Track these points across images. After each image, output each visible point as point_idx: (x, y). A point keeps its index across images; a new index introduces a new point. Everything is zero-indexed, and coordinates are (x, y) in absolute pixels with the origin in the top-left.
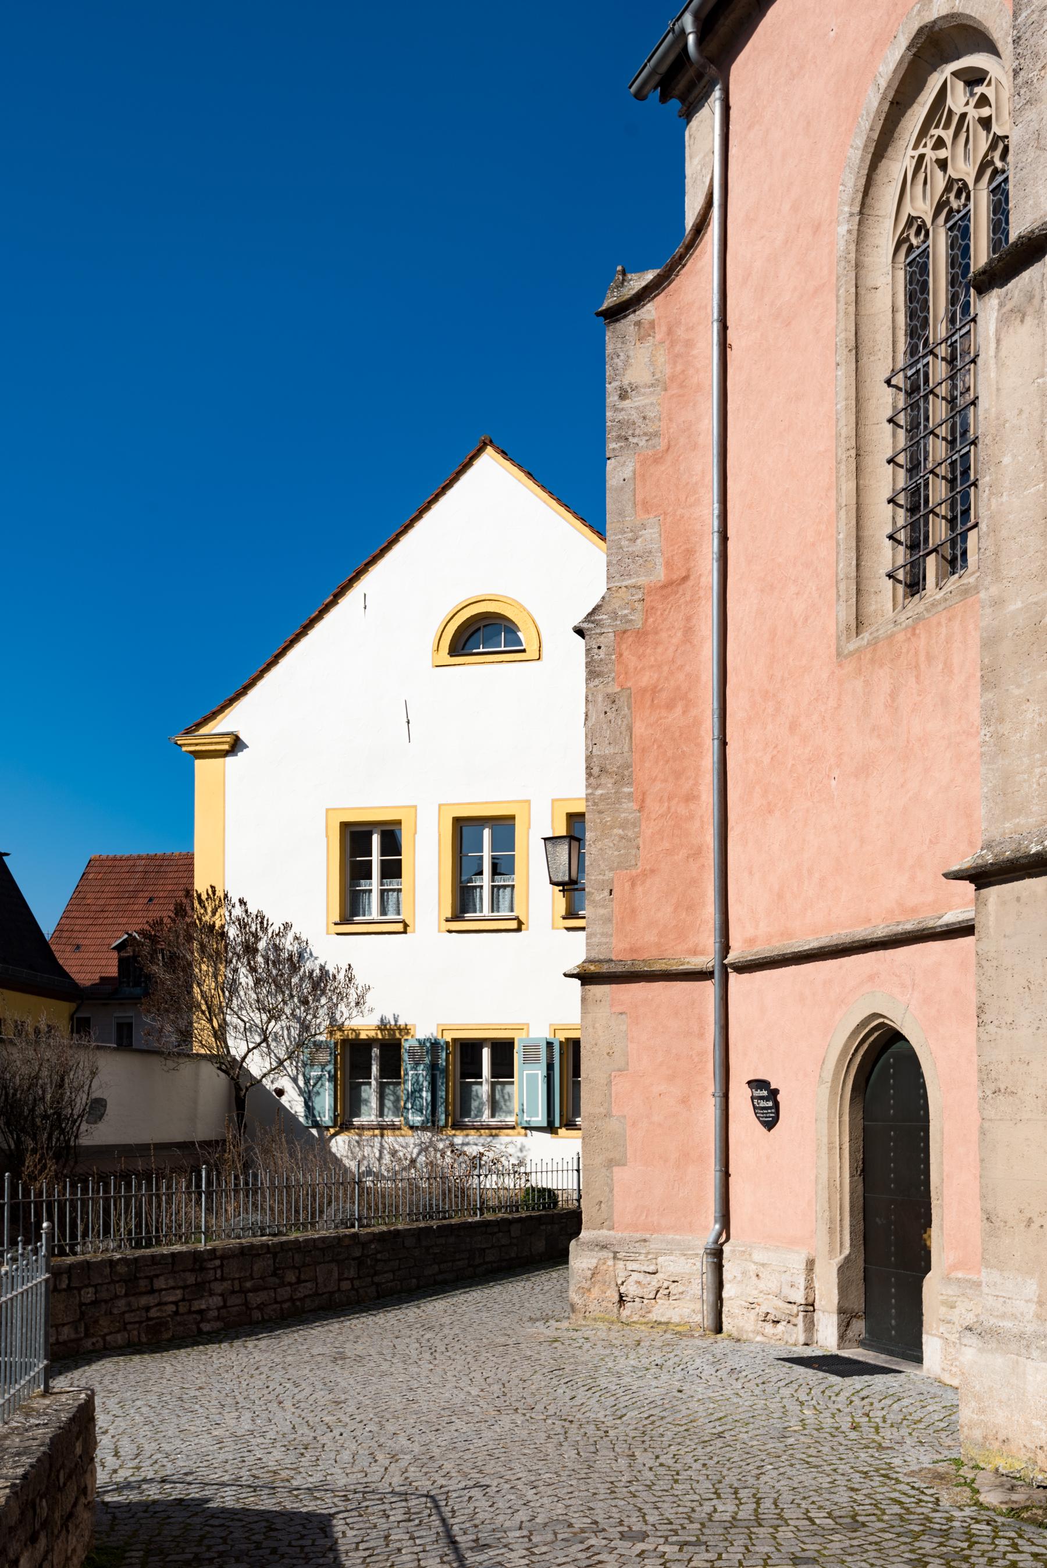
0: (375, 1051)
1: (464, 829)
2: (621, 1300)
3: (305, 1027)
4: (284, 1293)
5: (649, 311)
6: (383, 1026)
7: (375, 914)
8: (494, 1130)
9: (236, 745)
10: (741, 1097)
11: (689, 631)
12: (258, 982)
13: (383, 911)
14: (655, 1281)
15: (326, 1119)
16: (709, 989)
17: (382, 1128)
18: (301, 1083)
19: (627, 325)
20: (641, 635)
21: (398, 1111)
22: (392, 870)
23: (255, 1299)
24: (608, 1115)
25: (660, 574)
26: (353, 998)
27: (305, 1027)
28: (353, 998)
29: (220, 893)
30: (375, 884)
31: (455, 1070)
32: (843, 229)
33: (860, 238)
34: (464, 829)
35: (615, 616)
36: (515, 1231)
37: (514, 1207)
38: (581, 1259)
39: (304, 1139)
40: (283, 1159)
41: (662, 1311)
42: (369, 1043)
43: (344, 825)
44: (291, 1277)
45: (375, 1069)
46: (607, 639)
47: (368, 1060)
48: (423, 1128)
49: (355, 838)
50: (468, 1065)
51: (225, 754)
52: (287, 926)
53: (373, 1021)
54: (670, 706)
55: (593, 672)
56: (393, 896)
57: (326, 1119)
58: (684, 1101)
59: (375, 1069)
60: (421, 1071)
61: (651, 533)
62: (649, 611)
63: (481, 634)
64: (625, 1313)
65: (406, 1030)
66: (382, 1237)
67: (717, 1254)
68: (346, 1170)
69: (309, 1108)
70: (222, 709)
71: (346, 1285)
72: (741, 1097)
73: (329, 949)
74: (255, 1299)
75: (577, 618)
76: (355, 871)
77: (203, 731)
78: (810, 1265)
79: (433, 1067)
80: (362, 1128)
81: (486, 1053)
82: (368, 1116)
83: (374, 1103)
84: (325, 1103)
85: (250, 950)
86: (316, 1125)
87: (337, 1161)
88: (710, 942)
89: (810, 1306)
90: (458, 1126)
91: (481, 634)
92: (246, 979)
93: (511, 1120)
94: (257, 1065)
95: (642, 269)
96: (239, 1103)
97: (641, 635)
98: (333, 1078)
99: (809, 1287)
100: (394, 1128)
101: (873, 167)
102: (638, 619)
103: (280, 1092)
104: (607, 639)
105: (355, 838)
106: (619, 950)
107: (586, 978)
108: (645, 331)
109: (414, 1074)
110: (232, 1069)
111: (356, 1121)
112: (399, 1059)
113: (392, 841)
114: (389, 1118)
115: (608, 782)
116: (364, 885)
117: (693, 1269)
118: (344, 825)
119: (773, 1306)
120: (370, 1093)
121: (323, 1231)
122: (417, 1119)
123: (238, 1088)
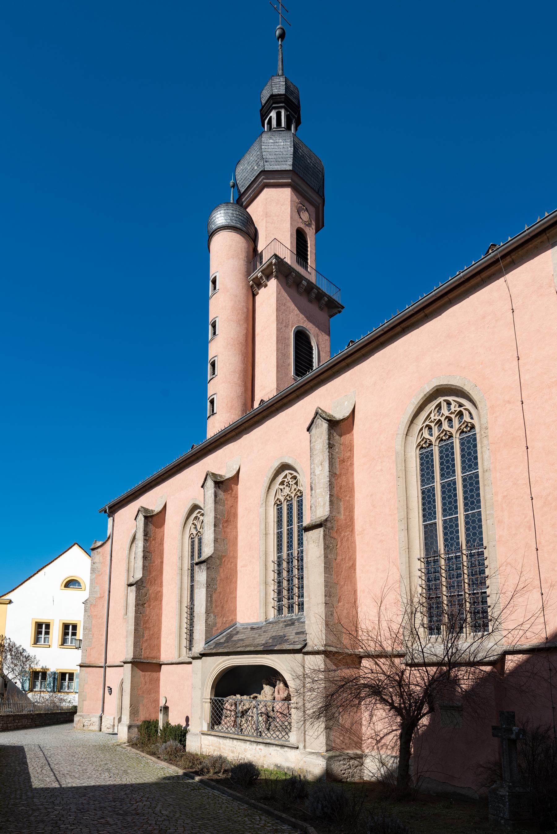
0: (40, 674)
1: (66, 627)
2: (84, 726)
3: (23, 668)
4: (15, 724)
5: (99, 550)
6: (42, 668)
7: (42, 642)
8: (68, 693)
9: (10, 602)
10: (107, 689)
11: (103, 606)
12: (12, 658)
13: (45, 642)
14: (90, 722)
15: (27, 689)
16: (103, 669)
17: (40, 691)
18: (21, 680)
19: (95, 551)
20: (95, 605)
21: (45, 688)
22: (47, 633)
23: (9, 725)
24: (83, 692)
25: (99, 595)
26: (35, 662)
27: (23, 668)
28: (35, 662)
29: (4, 637)
30: (43, 635)
31: (59, 679)
32: (127, 552)
33: (129, 554)
34: (66, 627)
35: (90, 601)
36: (68, 714)
37: (70, 709)
38: (76, 718)
39: (21, 694)
40: (16, 698)
41: (91, 728)
42: (38, 672)
43: (36, 622)
44: (17, 721)
45: (40, 678)
46: (88, 605)
47: (39, 676)
48: (51, 692)
49: (39, 625)
50: (63, 679)
51: (8, 604)
52: (20, 646)
53: (41, 667)
54: (99, 619)
55: (85, 611)
56: (47, 639)
57: (27, 689)
58: (98, 689)
59: (40, 678)
60: (51, 679)
61: (97, 588)
62: (96, 602)
63: (71, 583)
64: (84, 728)
65: (48, 669)
66: (37, 714)
67: (101, 717)
68: (30, 700)
69: (23, 686)
70: (7, 594)
71: (29, 724)
72: (107, 689)
73: (31, 651)
74: (9, 725)
75: (83, 601)
76: (39, 633)
77: (2, 598)
78: (114, 718)
79: (54, 678)
80: (36, 691)
81: (67, 675)
82: (37, 689)
83: (39, 686)
84: (27, 686)
85: (11, 650)
86: (24, 690)
87: (29, 699)
88: (103, 661)
89: (114, 725)
90: (59, 692)
91: (71, 583)
92: (9, 657)
93: (72, 691)
94: (10, 676)
95: (99, 541)
96: (6, 685)
97: (95, 605)
98: (29, 680)
99: (114, 722)
100: (43, 691)
101: (131, 544)
102: (94, 602)
103: (16, 683)
104: (88, 605)
105: (39, 625)
106: (87, 662)
107: (81, 666)
108: (98, 553)
109: (49, 680)
110: (4, 677)
111: (34, 690)
112: (46, 675)
113: (48, 626)
114: (43, 689)
115: (87, 631)
116: (40, 636)
117: (96, 720)
118: (36, 622)
119: (108, 726)
120: (38, 683)
121: (24, 713)
122: (50, 690)
123: (5, 681)
